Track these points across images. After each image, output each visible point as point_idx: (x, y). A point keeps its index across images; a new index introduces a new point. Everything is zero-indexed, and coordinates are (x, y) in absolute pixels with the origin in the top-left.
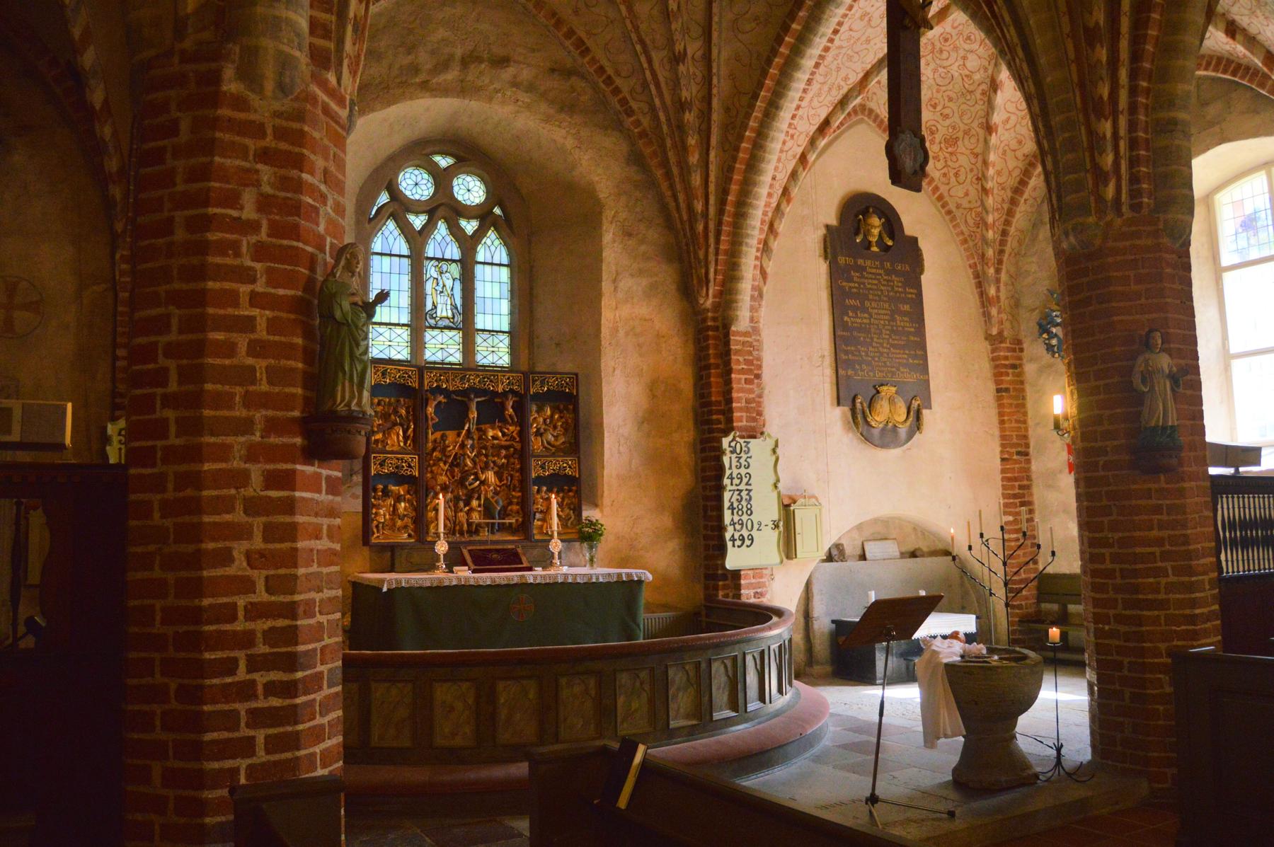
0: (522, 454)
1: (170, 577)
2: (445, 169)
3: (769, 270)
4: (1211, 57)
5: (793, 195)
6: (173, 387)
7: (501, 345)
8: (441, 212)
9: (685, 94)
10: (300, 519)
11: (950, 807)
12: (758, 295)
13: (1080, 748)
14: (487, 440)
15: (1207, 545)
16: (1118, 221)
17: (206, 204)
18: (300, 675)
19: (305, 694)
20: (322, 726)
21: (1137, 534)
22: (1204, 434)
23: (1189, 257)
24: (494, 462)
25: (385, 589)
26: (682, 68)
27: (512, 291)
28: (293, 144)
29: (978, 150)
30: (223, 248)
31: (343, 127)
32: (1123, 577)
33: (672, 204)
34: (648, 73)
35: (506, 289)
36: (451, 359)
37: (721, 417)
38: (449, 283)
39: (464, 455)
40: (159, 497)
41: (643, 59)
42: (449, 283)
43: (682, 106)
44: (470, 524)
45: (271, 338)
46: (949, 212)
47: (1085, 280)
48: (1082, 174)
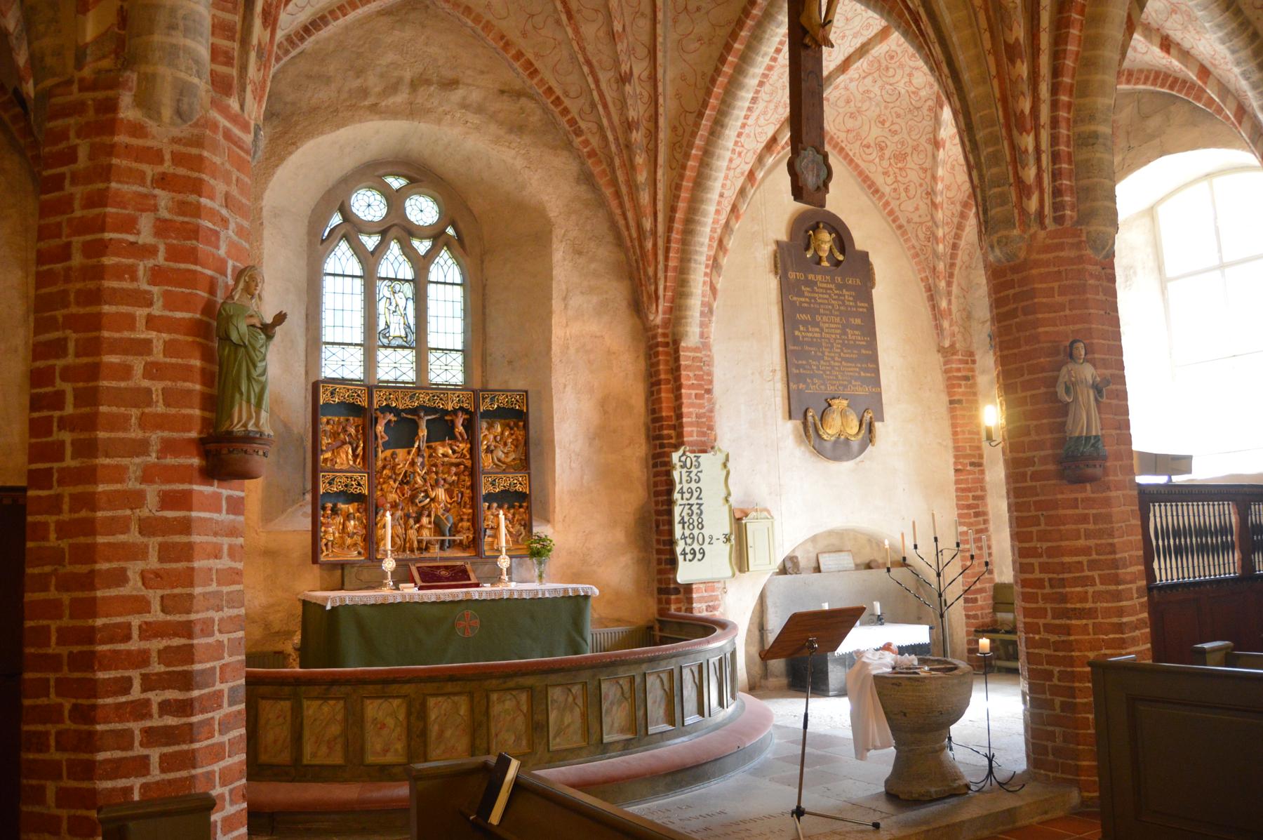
1: (66, 597)
2: (397, 191)
3: (719, 286)
4: (1149, 71)
5: (742, 211)
6: (69, 409)
7: (454, 363)
9: (632, 114)
10: (196, 538)
11: (876, 818)
12: (708, 311)
13: (1014, 759)
14: (437, 457)
15: (1135, 553)
16: (1042, 234)
17: (103, 229)
18: (196, 693)
19: (202, 712)
20: (222, 745)
21: (1064, 543)
22: (1130, 443)
23: (1113, 268)
24: (445, 480)
25: (328, 607)
26: (628, 88)
27: (465, 310)
28: (192, 169)
29: (926, 165)
30: (119, 272)
31: (247, 152)
32: (1052, 587)
33: (621, 222)
34: (595, 93)
35: (459, 307)
37: (672, 432)
38: (402, 303)
39: (414, 473)
40: (54, 518)
41: (590, 79)
42: (402, 303)
43: (629, 126)
44: (420, 542)
45: (168, 360)
46: (900, 227)
47: (1011, 292)
48: (1006, 188)
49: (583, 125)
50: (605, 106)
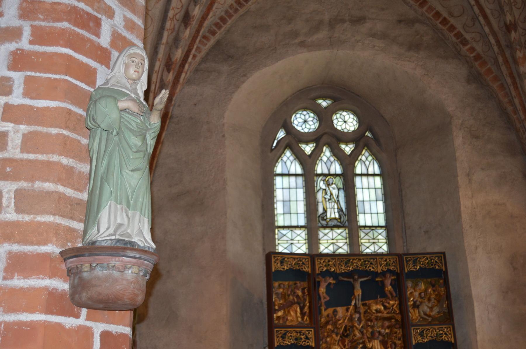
0: (404, 324)
2: (325, 108)
7: (380, 237)
8: (325, 139)
24: (379, 333)
34: (476, 8)
36: (340, 251)
38: (335, 192)
39: (353, 327)
42: (335, 192)
49: (468, 36)
50: (485, 17)
